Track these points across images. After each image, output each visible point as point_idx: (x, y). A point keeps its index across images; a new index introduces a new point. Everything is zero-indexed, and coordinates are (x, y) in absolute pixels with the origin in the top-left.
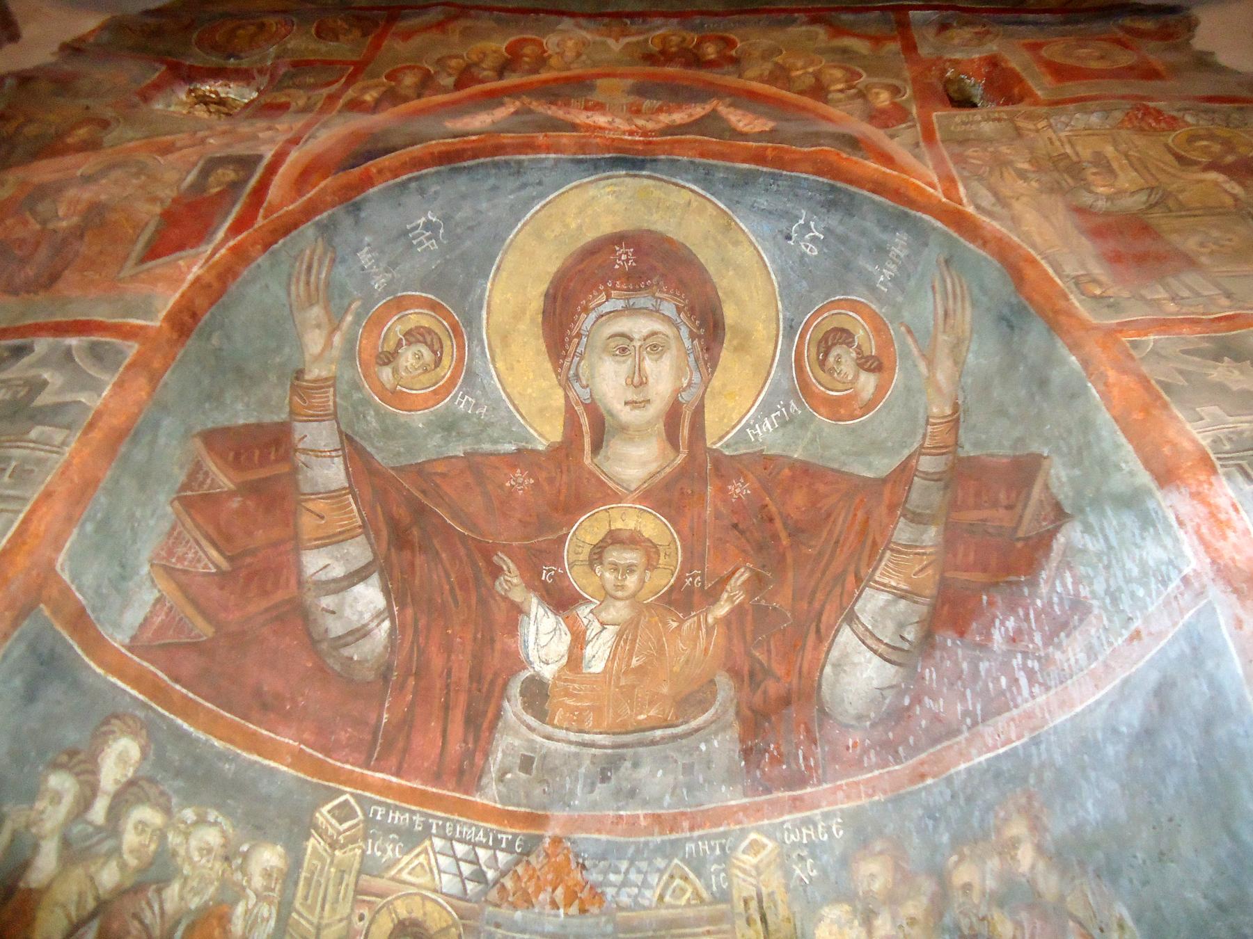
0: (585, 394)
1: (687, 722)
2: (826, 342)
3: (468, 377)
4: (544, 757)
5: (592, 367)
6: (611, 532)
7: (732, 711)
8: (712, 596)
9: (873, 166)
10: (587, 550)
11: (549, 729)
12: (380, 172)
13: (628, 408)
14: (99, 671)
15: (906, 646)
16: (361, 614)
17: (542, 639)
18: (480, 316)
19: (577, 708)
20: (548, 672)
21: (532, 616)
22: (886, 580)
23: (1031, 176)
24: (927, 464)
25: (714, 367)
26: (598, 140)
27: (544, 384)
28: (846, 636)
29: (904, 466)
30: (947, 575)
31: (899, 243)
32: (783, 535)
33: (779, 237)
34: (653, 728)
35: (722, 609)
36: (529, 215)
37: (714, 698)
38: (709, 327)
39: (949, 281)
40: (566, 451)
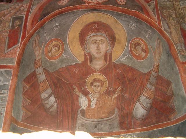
0: (88, 52)
1: (110, 117)
2: (136, 44)
3: (65, 51)
4: (85, 124)
5: (89, 46)
6: (94, 79)
7: (118, 115)
8: (114, 93)
9: (145, 16)
10: (90, 83)
11: (86, 119)
12: (47, 19)
13: (97, 54)
14: (19, 127)
15: (148, 107)
16: (52, 103)
17: (83, 102)
18: (67, 39)
19: (91, 115)
20: (85, 108)
21: (81, 98)
22: (145, 94)
23: (175, 19)
24: (153, 73)
25: (114, 46)
26: (90, 6)
27: (80, 50)
28: (138, 103)
29: (149, 72)
30: (155, 96)
31: (150, 32)
32: (127, 81)
33: (127, 25)
34: (104, 118)
35: (116, 95)
36: (76, 20)
37: (115, 112)
38: (113, 39)
39: (159, 41)
40: (85, 63)
